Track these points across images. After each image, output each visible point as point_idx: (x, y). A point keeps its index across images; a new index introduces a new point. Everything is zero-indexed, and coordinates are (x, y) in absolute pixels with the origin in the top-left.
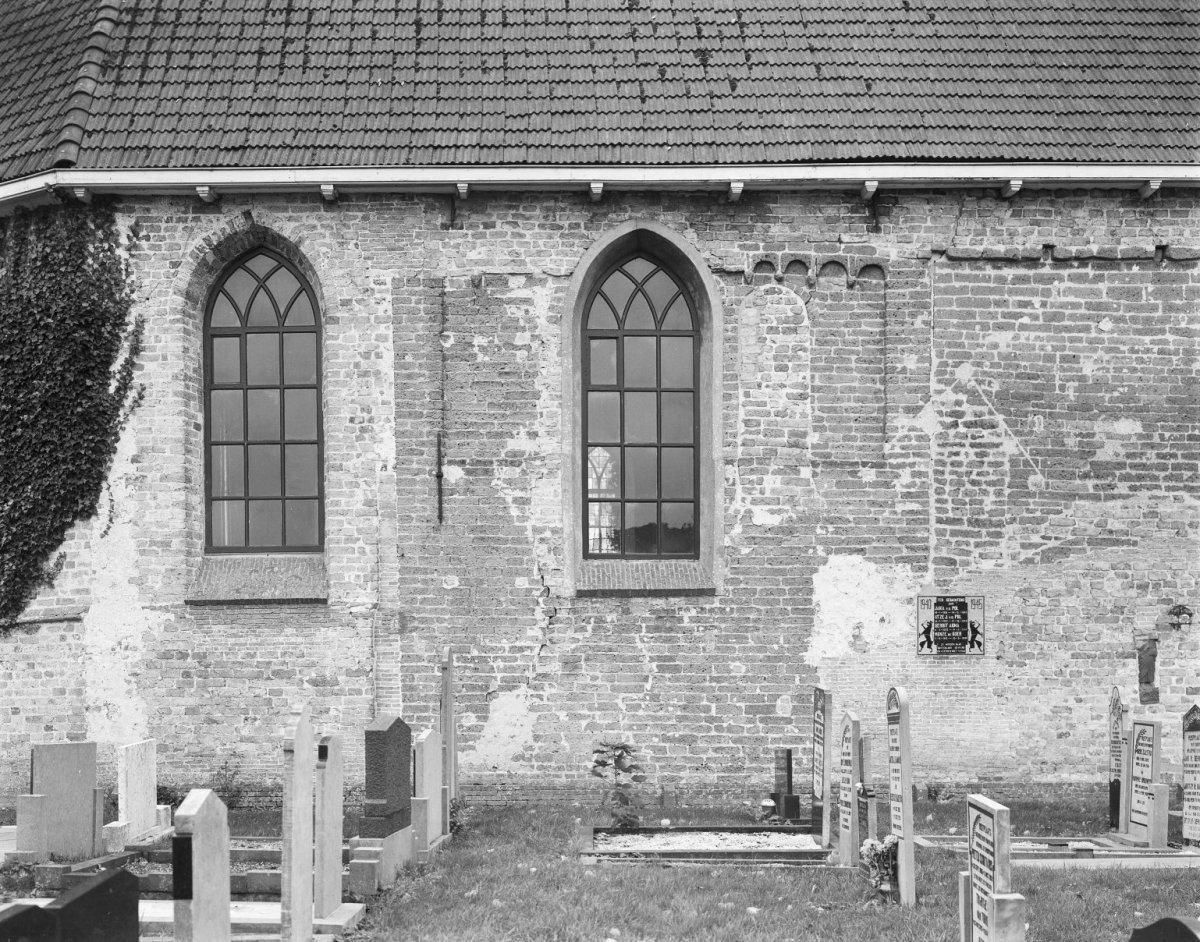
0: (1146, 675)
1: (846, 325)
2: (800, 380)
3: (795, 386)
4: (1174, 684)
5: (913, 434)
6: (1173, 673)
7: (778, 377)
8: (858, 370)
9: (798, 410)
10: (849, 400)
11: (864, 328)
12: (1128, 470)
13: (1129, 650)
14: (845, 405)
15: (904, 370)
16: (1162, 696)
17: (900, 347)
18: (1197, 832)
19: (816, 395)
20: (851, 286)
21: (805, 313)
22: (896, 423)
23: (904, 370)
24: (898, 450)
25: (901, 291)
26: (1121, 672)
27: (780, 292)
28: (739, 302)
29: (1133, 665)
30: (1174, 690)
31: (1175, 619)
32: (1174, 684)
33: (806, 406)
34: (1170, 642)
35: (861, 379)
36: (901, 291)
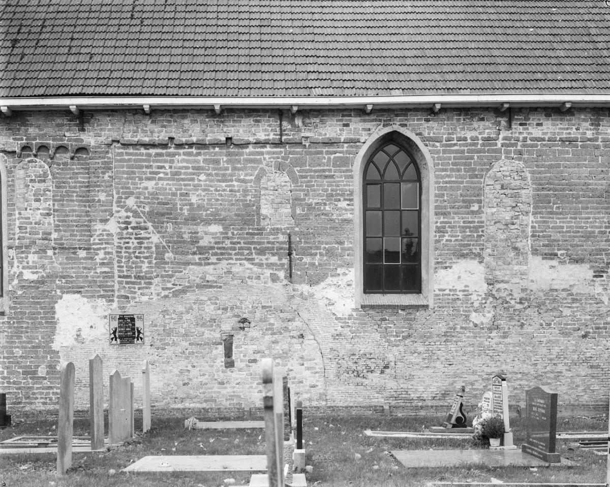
0: (228, 353)
1: (70, 178)
2: (47, 206)
3: (44, 209)
4: (242, 358)
5: (104, 233)
6: (241, 352)
8: (77, 201)
10: (73, 216)
11: (79, 179)
13: (219, 340)
16: (236, 364)
17: (97, 189)
23: (99, 201)
24: (97, 241)
25: (97, 161)
26: (214, 352)
29: (221, 349)
30: (241, 361)
31: (242, 325)
32: (242, 358)
34: (239, 336)
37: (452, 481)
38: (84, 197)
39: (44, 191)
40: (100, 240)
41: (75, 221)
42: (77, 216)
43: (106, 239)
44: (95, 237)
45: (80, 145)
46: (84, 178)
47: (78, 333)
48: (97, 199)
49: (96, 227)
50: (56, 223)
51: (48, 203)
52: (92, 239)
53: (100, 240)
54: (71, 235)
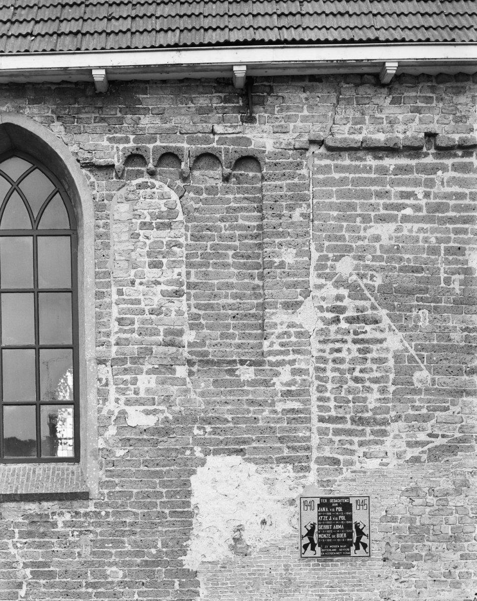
1: (222, 220)
2: (175, 277)
5: (292, 330)
7: (151, 274)
10: (226, 297)
11: (240, 222)
17: (277, 241)
22: (275, 319)
23: (282, 265)
24: (277, 347)
36: (278, 183)
40: (282, 345)
41: (231, 307)
42: (235, 296)
44: (273, 338)
45: (244, 150)
46: (248, 219)
48: (277, 260)
49: (275, 319)
50: (194, 310)
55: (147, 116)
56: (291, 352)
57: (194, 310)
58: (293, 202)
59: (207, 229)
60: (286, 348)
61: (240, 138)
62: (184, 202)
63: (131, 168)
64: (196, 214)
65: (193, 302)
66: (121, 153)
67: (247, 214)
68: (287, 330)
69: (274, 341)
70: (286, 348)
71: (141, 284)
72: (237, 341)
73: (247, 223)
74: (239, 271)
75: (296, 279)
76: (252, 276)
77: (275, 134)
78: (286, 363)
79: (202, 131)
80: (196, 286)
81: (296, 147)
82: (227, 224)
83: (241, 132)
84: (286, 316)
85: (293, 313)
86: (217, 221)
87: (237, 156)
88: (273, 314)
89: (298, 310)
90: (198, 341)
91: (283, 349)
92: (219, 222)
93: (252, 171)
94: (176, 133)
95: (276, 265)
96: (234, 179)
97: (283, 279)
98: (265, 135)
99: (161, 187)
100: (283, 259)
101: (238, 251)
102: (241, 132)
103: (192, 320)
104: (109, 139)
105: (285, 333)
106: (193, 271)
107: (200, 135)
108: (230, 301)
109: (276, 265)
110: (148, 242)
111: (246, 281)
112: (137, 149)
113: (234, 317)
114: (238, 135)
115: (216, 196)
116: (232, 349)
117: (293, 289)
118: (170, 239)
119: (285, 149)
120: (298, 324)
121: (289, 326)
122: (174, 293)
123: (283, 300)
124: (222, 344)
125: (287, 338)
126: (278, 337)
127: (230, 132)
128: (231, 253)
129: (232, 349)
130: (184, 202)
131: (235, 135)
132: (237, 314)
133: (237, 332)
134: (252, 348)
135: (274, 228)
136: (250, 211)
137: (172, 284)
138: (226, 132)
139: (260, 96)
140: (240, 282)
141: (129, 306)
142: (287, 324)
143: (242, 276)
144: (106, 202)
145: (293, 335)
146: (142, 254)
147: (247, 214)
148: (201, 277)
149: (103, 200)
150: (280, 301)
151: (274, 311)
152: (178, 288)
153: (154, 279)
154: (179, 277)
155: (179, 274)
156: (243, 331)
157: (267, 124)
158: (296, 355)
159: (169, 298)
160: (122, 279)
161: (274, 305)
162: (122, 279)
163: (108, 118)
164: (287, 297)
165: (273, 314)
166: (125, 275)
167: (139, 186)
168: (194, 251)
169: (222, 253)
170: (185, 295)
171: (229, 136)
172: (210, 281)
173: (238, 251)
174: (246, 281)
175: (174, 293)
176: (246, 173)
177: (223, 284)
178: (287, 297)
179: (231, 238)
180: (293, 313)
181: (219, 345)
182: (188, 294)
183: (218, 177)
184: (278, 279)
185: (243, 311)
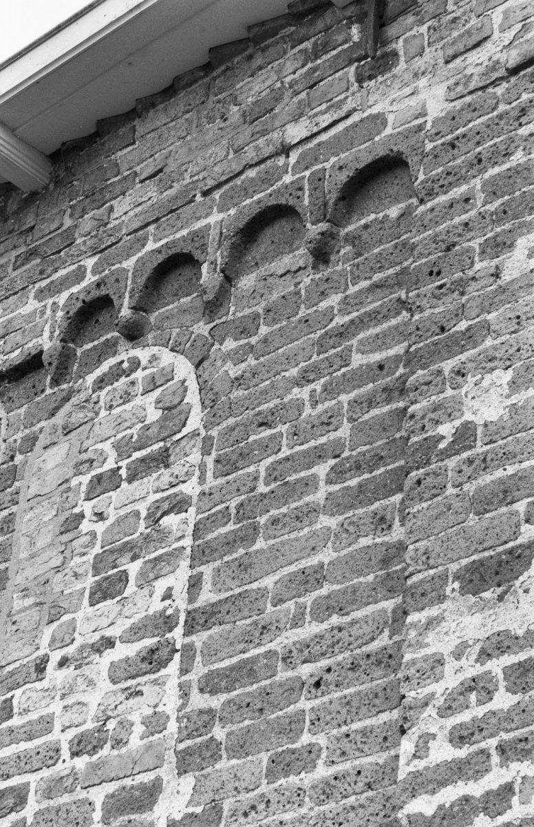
1: (304, 379)
2: (157, 605)
3: (136, 633)
5: (497, 666)
7: (89, 621)
8: (335, 505)
9: (138, 711)
10: (297, 621)
11: (357, 360)
12: (348, 94)
14: (290, 637)
15: (465, 435)
17: (448, 366)
18: (531, 811)
19: (199, 639)
20: (321, 255)
21: (193, 397)
22: (438, 644)
23: (465, 435)
24: (443, 752)
25: (458, 191)
27: (135, 364)
28: (31, 441)
33: (166, 692)
35: (350, 531)
36: (458, 191)
37: (518, 441)
38: (379, 459)
39: (154, 518)
40: (460, 737)
41: (307, 652)
42: (324, 609)
43: (505, 719)
44: (429, 721)
45: (363, 153)
46: (379, 342)
47: (170, 317)
48: (446, 430)
49: (438, 644)
50: (199, 701)
51: (161, 586)
52: (407, 746)
53: (460, 737)
54: (281, 765)
55: (127, 194)
56: (495, 759)
57: (199, 701)
58: (507, 226)
59: (261, 425)
60: (475, 748)
61: (355, 125)
62: (206, 376)
63: (90, 346)
64: (238, 393)
65: (199, 670)
66: (60, 314)
67: (378, 330)
68: (478, 670)
69: (433, 730)
70: (475, 748)
71: (63, 663)
72: (322, 771)
73: (377, 357)
74: (341, 518)
75: (511, 470)
76: (383, 519)
77: (451, 66)
78: (475, 811)
79: (256, 160)
80: (214, 613)
81: (512, 63)
82: (318, 386)
83: (355, 110)
84: (477, 618)
85: (501, 598)
86: (288, 390)
87: (343, 177)
88: (431, 624)
89: (517, 583)
90: (198, 810)
91: (462, 753)
92: (296, 390)
93: (397, 200)
94: (192, 201)
95: (442, 446)
96: (347, 249)
97: (466, 487)
98: (423, 82)
99: (154, 358)
100: (468, 416)
101: (346, 454)
102: (355, 110)
103: (189, 737)
104: (40, 295)
105: (473, 685)
106: (207, 570)
107: (251, 173)
108: (311, 629)
109: (442, 446)
110: (100, 528)
111: (364, 542)
112: (98, 285)
113: (317, 685)
114: (349, 122)
115: (293, 319)
116: (303, 811)
117: (504, 509)
118: (159, 496)
119: (483, 88)
120: (520, 633)
121: (485, 655)
122: (143, 659)
123: (464, 562)
124: (274, 797)
125: (480, 703)
126: (446, 710)
127: (324, 125)
128: (322, 470)
129: (303, 811)
130: (206, 376)
131: (340, 127)
132: (329, 670)
133: (321, 740)
134: (369, 786)
135: (443, 329)
136: (386, 318)
137: (141, 633)
138: (315, 130)
139: (521, 43)
140: (345, 552)
141: (24, 746)
142: (478, 648)
143: (352, 529)
144: (19, 458)
145: (502, 684)
146: (80, 571)
147: (378, 330)
148: (229, 583)
149: (12, 458)
150: (454, 567)
151: (434, 611)
152: (156, 639)
153: (97, 636)
154: (168, 602)
155: (168, 595)
156: (344, 729)
157: (427, 50)
158: (515, 766)
159: (130, 683)
160: (17, 664)
161: (432, 593)
162: (17, 664)
163: (43, 244)
164: (481, 545)
165: (431, 624)
166: (27, 650)
167: (101, 383)
168: (219, 508)
169: (298, 481)
170: (177, 656)
171: (324, 137)
172: (255, 586)
173: (346, 454)
174: (364, 542)
175: (143, 659)
176: (381, 215)
177: (291, 578)
178: (481, 545)
179: (328, 423)
180: (501, 598)
181: (261, 807)
182: (188, 650)
183: (301, 263)
184: (450, 491)
185: (347, 654)
